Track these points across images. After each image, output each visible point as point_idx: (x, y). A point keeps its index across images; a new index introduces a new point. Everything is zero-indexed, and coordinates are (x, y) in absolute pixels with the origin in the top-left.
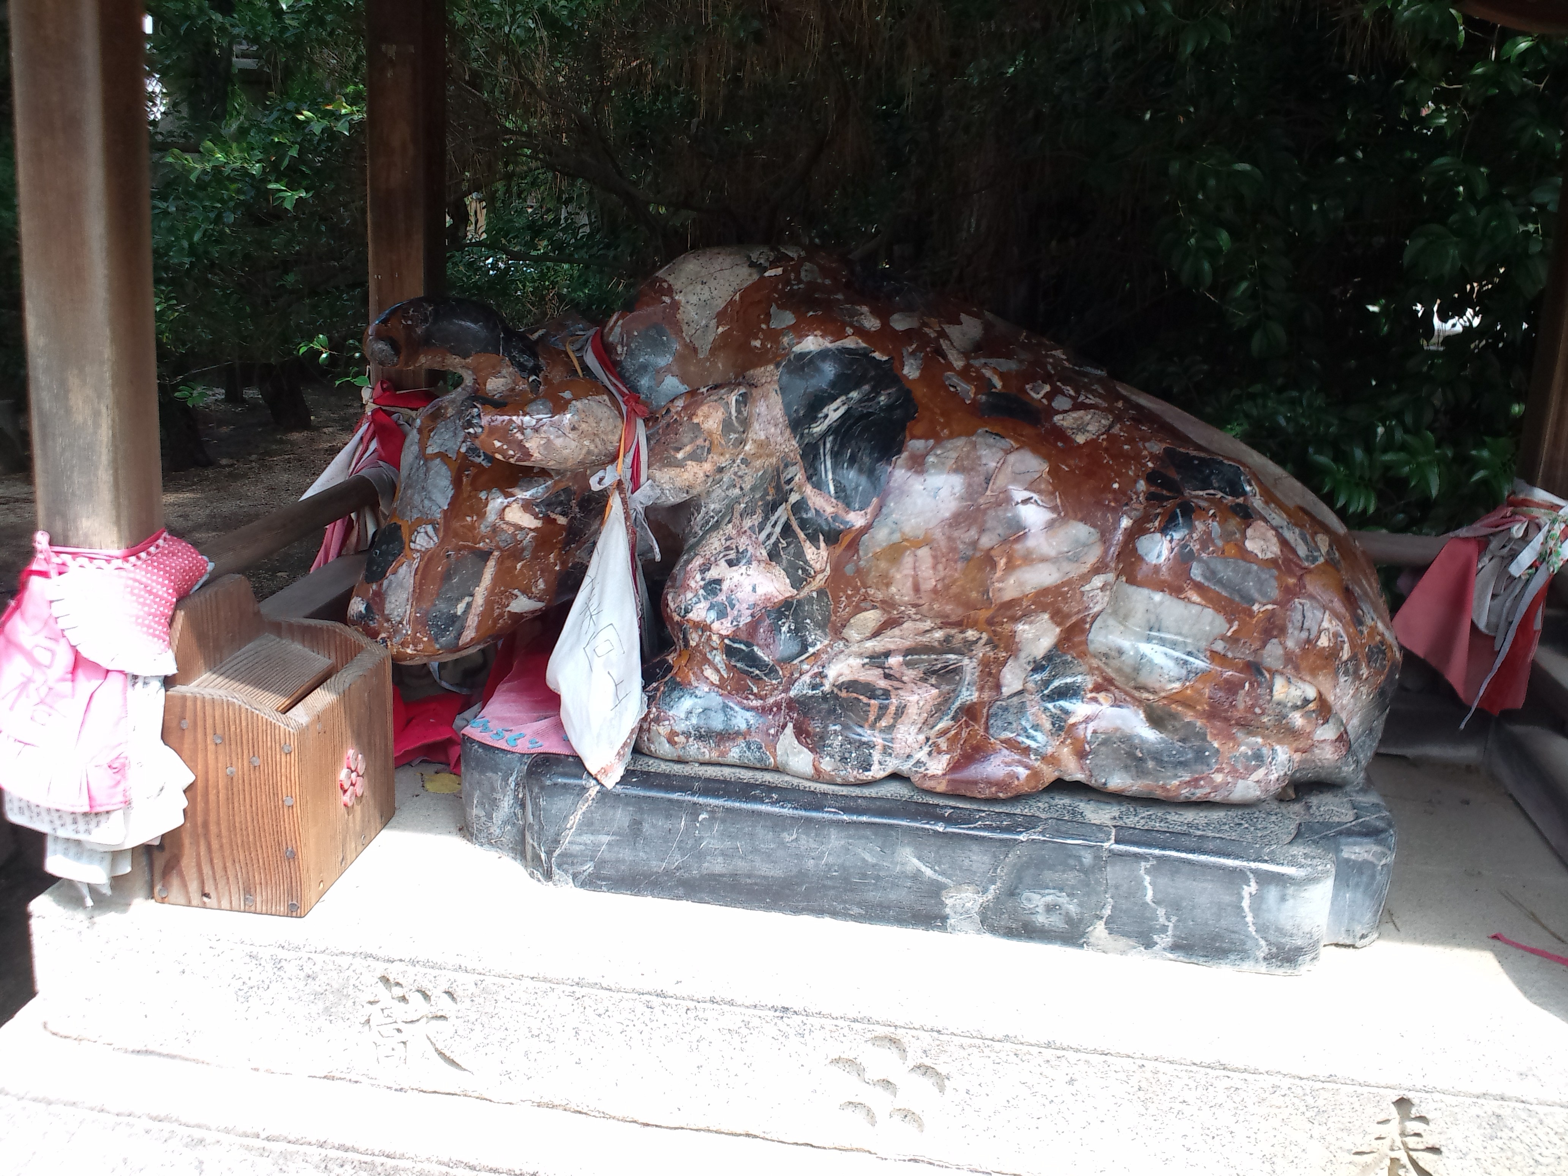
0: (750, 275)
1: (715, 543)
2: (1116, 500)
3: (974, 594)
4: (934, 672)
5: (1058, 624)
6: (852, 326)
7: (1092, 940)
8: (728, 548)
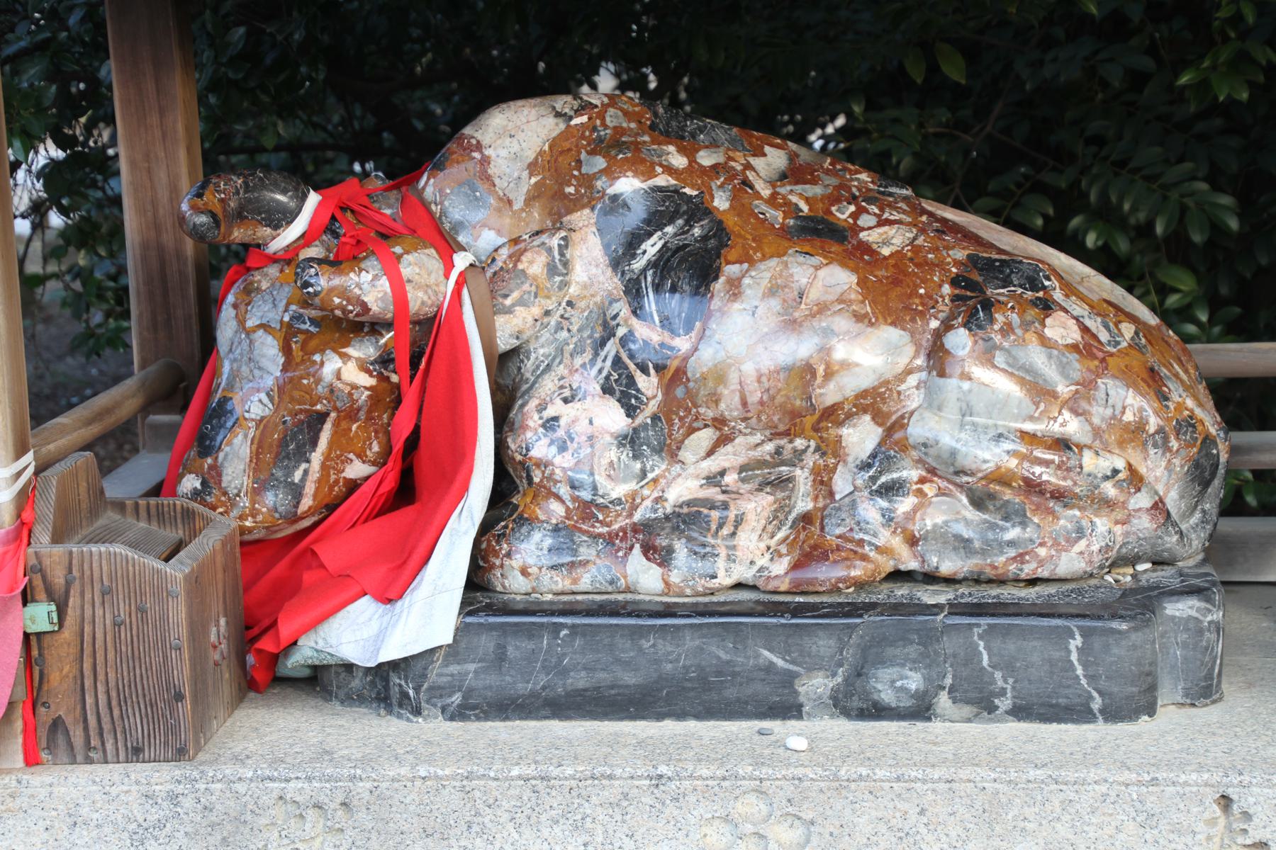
0: (557, 124)
1: (548, 385)
2: (923, 304)
3: (798, 403)
4: (769, 483)
5: (880, 425)
6: (661, 165)
7: (938, 711)
8: (562, 387)
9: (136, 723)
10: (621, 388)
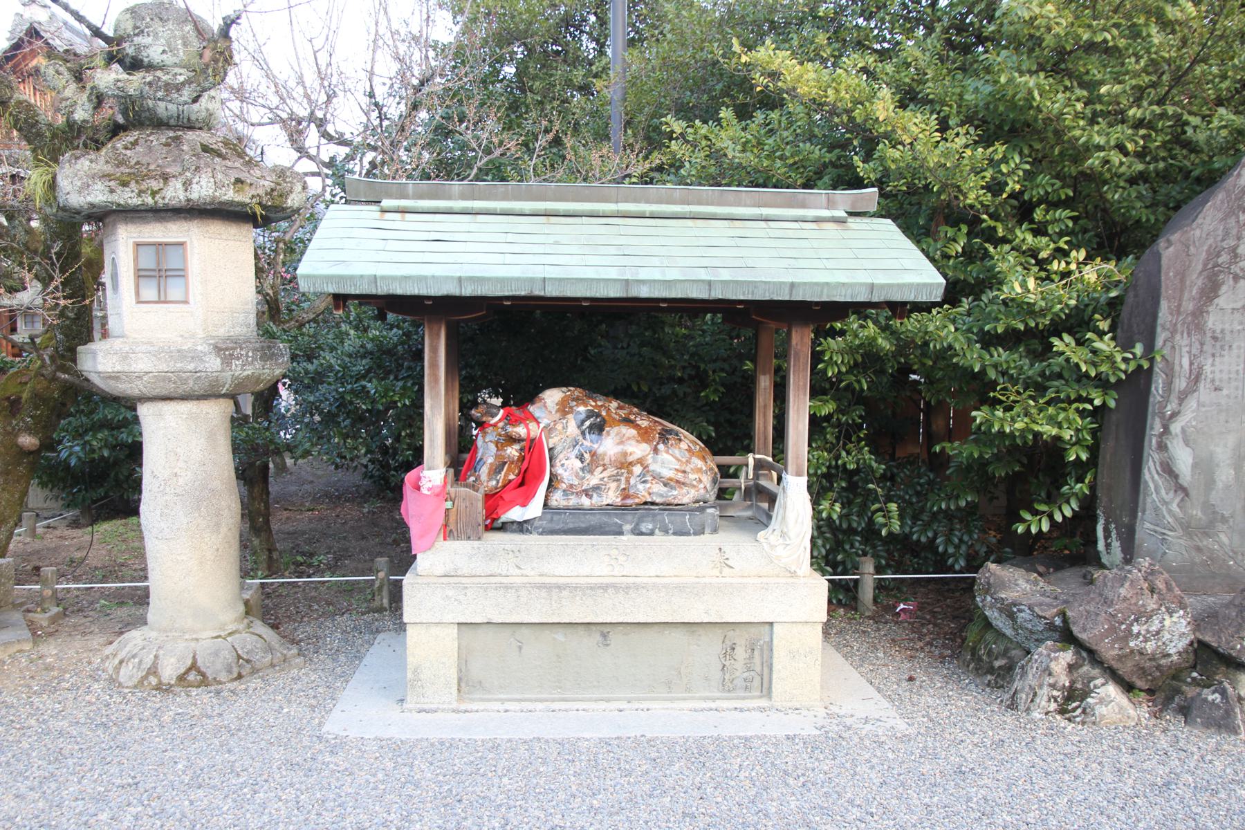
1: (561, 456)
9: (469, 531)
10: (581, 458)
